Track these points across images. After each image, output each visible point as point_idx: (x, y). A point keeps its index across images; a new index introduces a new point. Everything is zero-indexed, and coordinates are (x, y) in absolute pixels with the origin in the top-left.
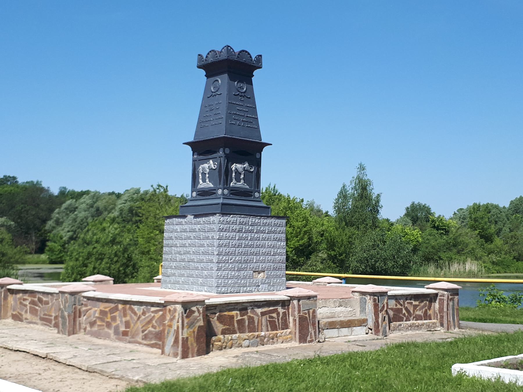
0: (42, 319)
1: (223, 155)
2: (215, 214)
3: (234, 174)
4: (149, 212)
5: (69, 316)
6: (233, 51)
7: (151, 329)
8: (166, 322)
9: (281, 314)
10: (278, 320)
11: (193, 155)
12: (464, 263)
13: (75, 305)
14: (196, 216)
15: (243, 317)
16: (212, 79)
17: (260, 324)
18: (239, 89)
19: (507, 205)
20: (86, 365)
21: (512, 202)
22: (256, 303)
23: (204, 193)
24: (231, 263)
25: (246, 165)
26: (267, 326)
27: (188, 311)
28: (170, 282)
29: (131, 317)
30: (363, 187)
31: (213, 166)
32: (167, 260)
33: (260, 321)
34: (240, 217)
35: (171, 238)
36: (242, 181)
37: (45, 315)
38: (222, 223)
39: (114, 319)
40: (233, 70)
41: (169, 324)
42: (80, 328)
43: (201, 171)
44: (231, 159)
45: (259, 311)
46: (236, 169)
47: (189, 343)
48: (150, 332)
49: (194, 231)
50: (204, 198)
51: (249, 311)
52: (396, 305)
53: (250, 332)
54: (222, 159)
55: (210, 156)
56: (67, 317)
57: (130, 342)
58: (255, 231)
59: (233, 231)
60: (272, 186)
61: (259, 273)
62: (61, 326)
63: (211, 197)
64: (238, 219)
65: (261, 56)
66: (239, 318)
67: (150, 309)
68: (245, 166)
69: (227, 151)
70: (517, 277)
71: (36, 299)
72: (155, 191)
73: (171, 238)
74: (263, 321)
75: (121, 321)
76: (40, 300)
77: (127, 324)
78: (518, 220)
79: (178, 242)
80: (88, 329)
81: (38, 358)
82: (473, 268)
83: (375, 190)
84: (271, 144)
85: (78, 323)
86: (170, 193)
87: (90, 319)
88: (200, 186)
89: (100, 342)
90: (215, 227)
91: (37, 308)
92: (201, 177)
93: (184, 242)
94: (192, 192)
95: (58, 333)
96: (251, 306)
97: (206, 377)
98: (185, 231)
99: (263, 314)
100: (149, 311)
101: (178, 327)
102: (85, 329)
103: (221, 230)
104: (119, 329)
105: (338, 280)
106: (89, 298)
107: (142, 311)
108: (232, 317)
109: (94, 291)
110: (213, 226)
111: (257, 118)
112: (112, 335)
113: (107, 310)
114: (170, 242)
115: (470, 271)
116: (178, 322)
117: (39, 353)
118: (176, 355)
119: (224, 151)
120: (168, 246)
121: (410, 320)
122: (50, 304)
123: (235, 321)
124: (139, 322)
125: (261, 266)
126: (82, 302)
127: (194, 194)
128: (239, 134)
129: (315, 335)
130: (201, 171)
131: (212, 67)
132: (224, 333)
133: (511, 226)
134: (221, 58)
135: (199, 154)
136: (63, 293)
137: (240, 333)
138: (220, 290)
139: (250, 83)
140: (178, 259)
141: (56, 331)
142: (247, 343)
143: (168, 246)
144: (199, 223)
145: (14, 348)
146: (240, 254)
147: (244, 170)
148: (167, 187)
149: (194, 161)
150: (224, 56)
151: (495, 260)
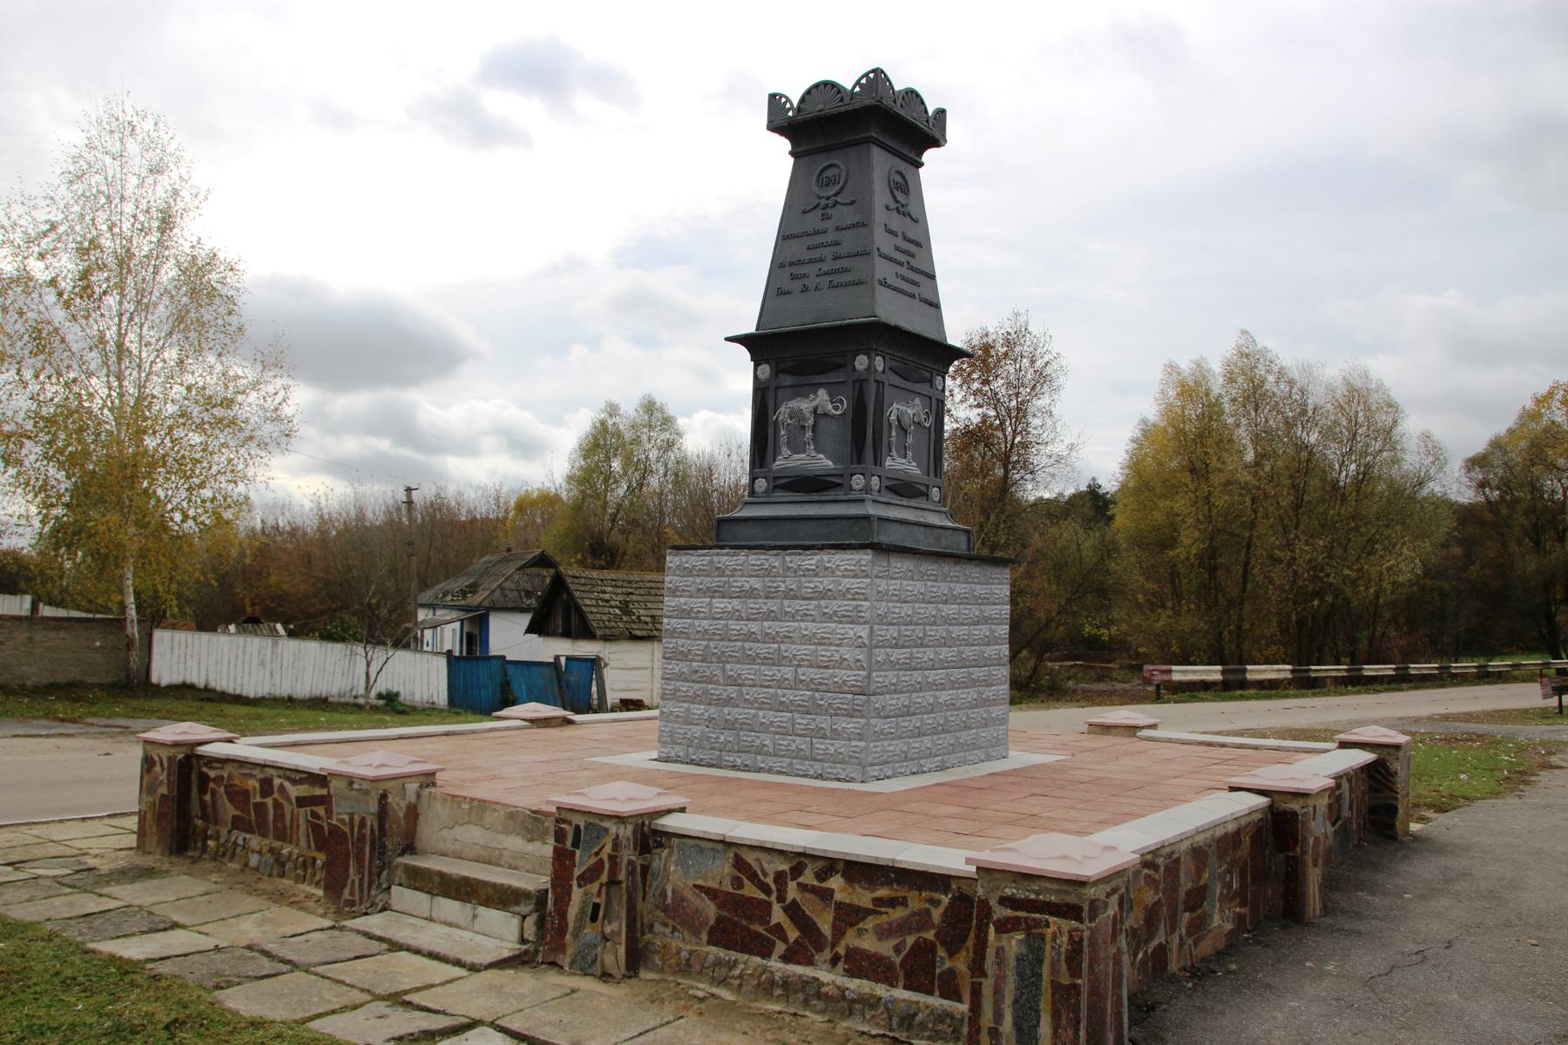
16: (822, 161)
50: (905, 502)
52: (738, 883)
55: (817, 379)
63: (913, 503)
84: (727, 339)
99: (302, 802)
121: (810, 962)
127: (761, 484)
129: (361, 891)
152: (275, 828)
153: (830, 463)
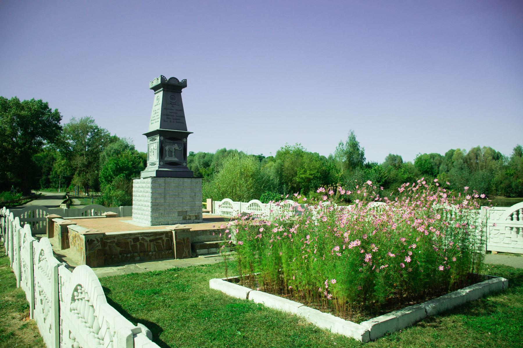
9: (165, 240)
10: (163, 244)
30: (354, 145)
40: (172, 89)
66: (132, 243)
74: (152, 245)
83: (361, 146)
97: (306, 304)
99: (151, 241)
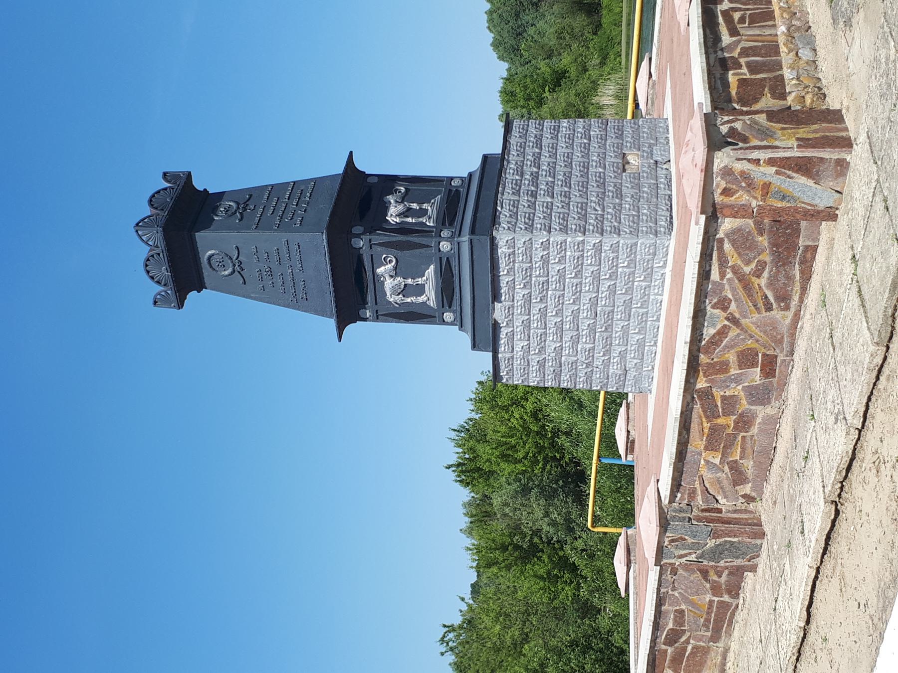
0: (715, 638)
1: (367, 237)
2: (493, 239)
3: (409, 220)
4: (488, 661)
5: (715, 534)
6: (149, 217)
7: (763, 281)
8: (754, 203)
10: (748, 9)
11: (365, 320)
12: (601, 108)
13: (690, 519)
14: (496, 297)
15: (743, 64)
16: (206, 272)
17: (759, 38)
18: (230, 213)
19: (506, 65)
20: (872, 348)
21: (501, 58)
22: (710, 44)
23: (448, 290)
24: (603, 210)
25: (391, 199)
26: (763, 26)
27: (729, 140)
28: (639, 367)
29: (729, 347)
31: (390, 266)
32: (589, 377)
33: (751, 38)
34: (503, 194)
35: (542, 364)
36: (425, 206)
37: (706, 625)
38: (515, 225)
39: (730, 403)
41: (759, 194)
42: (746, 511)
43: (399, 298)
44: (378, 223)
45: (726, 39)
46: (399, 215)
47: (811, 136)
48: (770, 284)
49: (528, 299)
50: (457, 290)
51: (727, 55)
53: (777, 53)
54: (376, 239)
55: (369, 274)
56: (719, 541)
57: (792, 353)
58: (535, 170)
59: (532, 205)
60: (453, 435)
61: (628, 163)
62: (739, 562)
63: (455, 271)
64: (507, 196)
65: (165, 174)
67: (715, 283)
68: (392, 201)
69: (358, 229)
70: (630, 24)
71: (670, 650)
72: (452, 649)
73: (542, 364)
75: (737, 380)
76: (672, 639)
77: (747, 359)
78: (530, 47)
79: (551, 346)
80: (747, 489)
81: (834, 535)
82: (611, 92)
84: (351, 153)
85: (736, 516)
86: (457, 620)
87: (725, 483)
88: (432, 303)
89: (783, 444)
90: (521, 239)
91: (690, 648)
92: (413, 299)
93: (551, 330)
94: (443, 322)
95: (753, 569)
96: (716, 52)
98: (527, 325)
99: (733, 32)
100: (719, 287)
101: (771, 162)
102: (749, 499)
103: (530, 228)
104: (756, 387)
105: (645, 64)
106: (676, 485)
107: (717, 311)
108: (742, 82)
109: (658, 481)
110: (519, 244)
111: (294, 182)
112: (769, 410)
113: (706, 425)
114: (549, 371)
115: (617, 97)
116: (757, 162)
117: (821, 529)
118: (842, 166)
119: (358, 236)
120: (558, 374)
122: (683, 607)
123: (753, 77)
124: (743, 321)
125: (611, 159)
126: (683, 505)
127: (448, 316)
128: (325, 208)
130: (399, 298)
131: (183, 274)
132: (783, 96)
133: (540, 57)
134: (162, 244)
135: (364, 302)
136: (660, 551)
137: (781, 68)
138: (662, 229)
139: (220, 195)
140: (588, 346)
141: (750, 574)
142: (805, 54)
143: (558, 374)
144: (512, 286)
145: (802, 624)
146: (584, 193)
147: (402, 202)
148: (445, 626)
149: (377, 318)
150: (156, 236)
151: (598, 61)
152: (766, 55)
153: (432, 267)
